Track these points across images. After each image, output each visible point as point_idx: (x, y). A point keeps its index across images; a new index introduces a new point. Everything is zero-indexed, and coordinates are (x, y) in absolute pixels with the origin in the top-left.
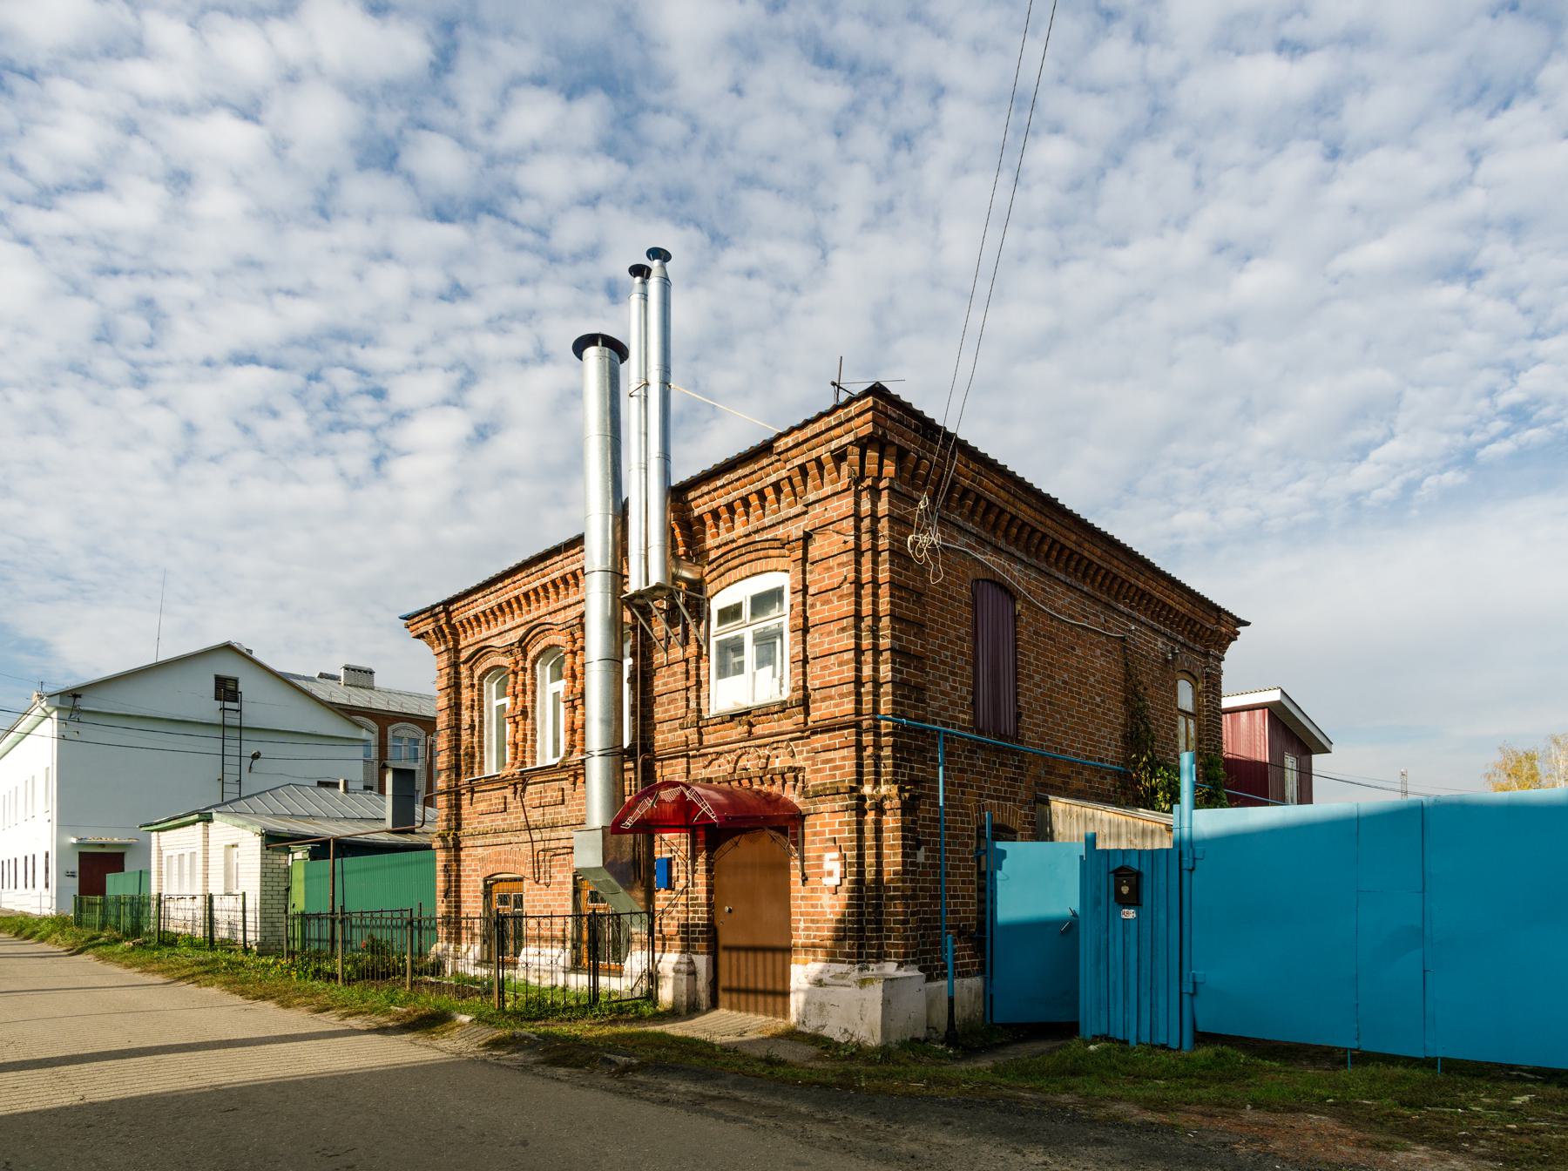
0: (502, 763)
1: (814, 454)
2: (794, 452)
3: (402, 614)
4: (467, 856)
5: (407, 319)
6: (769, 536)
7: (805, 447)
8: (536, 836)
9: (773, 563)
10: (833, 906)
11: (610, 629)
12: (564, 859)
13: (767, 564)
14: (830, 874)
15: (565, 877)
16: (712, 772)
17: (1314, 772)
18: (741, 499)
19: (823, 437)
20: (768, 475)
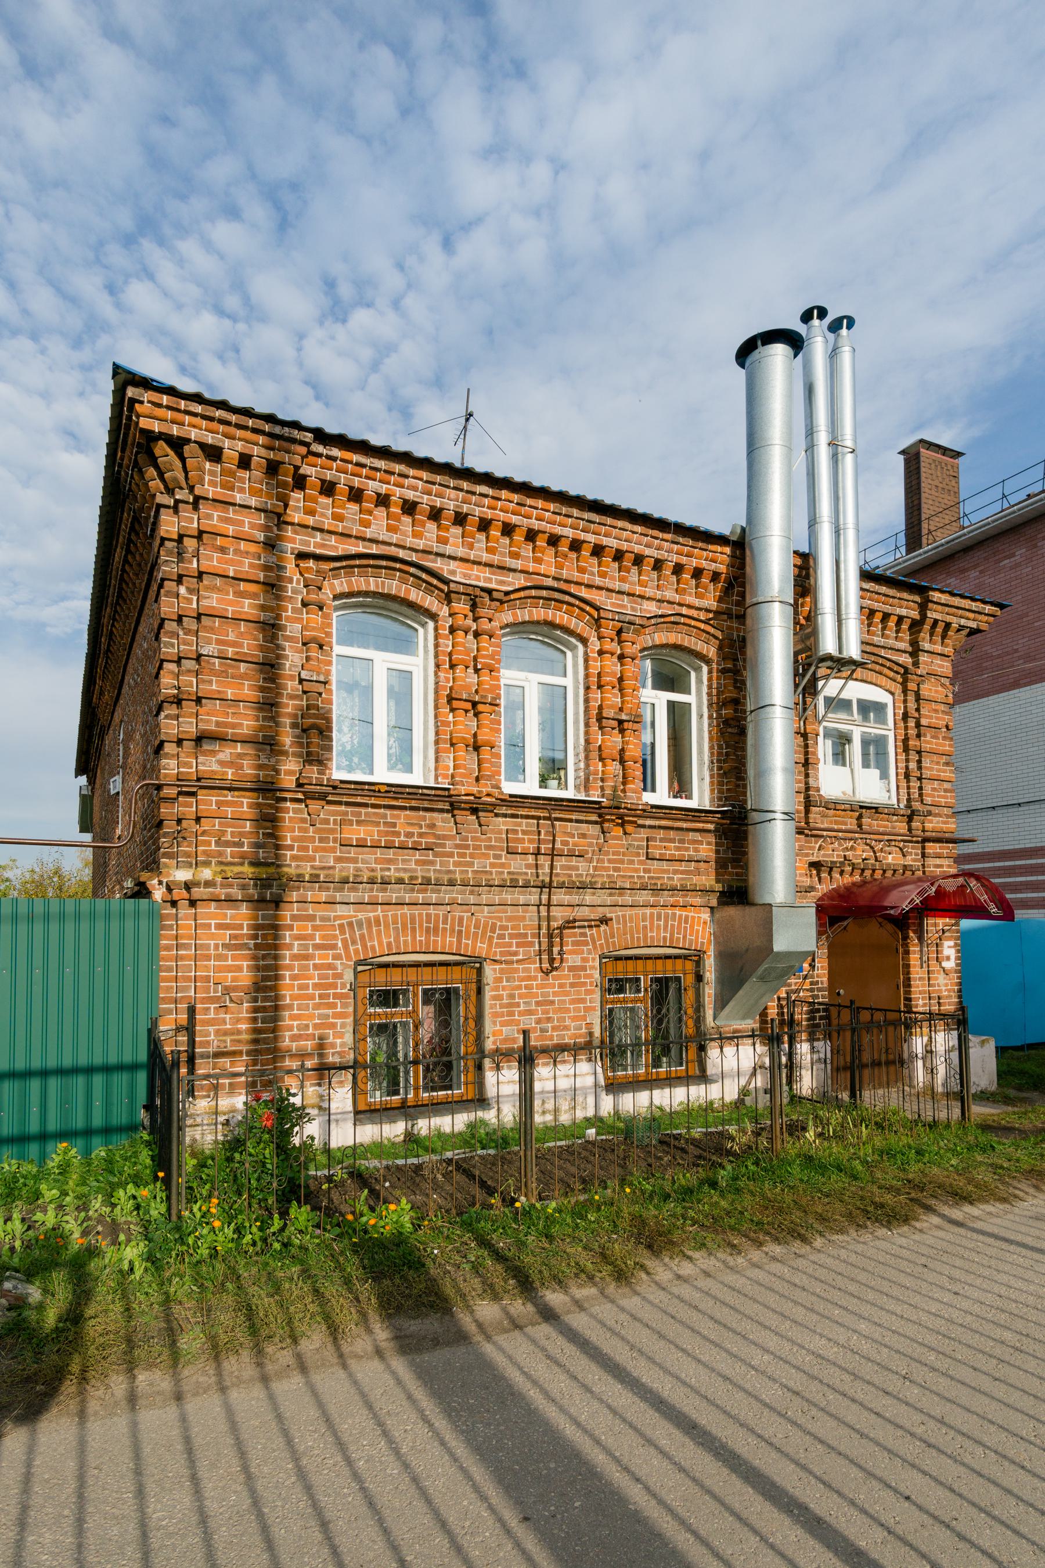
0: (403, 758)
1: (949, 618)
2: (940, 607)
3: (125, 362)
4: (294, 918)
5: (704, 156)
6: (894, 658)
7: (947, 609)
8: (559, 896)
9: (883, 680)
10: (946, 985)
11: (757, 660)
12: (584, 935)
13: (877, 678)
14: (948, 958)
15: (584, 960)
16: (824, 855)
17: (351, 1143)
18: (899, 616)
19: (960, 612)
20: (901, 607)
